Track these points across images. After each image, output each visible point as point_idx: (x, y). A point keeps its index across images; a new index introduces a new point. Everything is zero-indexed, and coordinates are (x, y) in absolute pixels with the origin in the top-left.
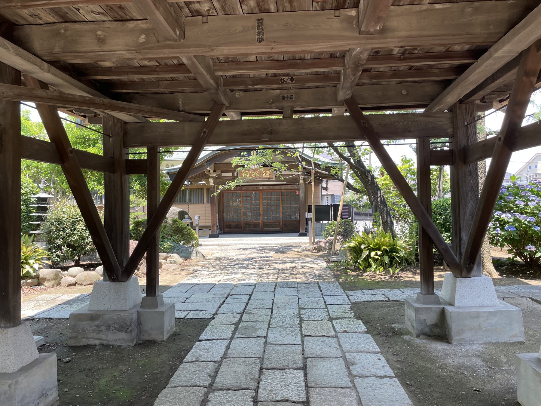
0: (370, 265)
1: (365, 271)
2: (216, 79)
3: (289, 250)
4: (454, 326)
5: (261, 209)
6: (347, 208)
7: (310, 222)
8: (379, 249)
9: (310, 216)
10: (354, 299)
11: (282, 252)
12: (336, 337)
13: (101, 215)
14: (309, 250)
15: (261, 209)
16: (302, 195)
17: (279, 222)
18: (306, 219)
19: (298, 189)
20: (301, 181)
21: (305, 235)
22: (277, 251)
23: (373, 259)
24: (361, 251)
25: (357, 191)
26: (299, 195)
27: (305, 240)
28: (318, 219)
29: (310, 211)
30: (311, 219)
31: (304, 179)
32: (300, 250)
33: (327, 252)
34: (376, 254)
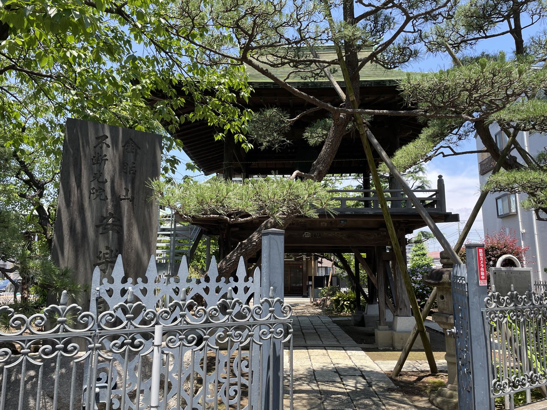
0: (344, 309)
1: (341, 312)
2: (28, 16)
6: (335, 279)
7: (310, 287)
13: (272, 81)
19: (302, 265)
20: (304, 259)
21: (307, 297)
23: (346, 305)
24: (340, 301)
25: (341, 268)
26: (302, 268)
27: (307, 300)
28: (316, 286)
30: (311, 285)
32: (304, 305)
33: (322, 305)
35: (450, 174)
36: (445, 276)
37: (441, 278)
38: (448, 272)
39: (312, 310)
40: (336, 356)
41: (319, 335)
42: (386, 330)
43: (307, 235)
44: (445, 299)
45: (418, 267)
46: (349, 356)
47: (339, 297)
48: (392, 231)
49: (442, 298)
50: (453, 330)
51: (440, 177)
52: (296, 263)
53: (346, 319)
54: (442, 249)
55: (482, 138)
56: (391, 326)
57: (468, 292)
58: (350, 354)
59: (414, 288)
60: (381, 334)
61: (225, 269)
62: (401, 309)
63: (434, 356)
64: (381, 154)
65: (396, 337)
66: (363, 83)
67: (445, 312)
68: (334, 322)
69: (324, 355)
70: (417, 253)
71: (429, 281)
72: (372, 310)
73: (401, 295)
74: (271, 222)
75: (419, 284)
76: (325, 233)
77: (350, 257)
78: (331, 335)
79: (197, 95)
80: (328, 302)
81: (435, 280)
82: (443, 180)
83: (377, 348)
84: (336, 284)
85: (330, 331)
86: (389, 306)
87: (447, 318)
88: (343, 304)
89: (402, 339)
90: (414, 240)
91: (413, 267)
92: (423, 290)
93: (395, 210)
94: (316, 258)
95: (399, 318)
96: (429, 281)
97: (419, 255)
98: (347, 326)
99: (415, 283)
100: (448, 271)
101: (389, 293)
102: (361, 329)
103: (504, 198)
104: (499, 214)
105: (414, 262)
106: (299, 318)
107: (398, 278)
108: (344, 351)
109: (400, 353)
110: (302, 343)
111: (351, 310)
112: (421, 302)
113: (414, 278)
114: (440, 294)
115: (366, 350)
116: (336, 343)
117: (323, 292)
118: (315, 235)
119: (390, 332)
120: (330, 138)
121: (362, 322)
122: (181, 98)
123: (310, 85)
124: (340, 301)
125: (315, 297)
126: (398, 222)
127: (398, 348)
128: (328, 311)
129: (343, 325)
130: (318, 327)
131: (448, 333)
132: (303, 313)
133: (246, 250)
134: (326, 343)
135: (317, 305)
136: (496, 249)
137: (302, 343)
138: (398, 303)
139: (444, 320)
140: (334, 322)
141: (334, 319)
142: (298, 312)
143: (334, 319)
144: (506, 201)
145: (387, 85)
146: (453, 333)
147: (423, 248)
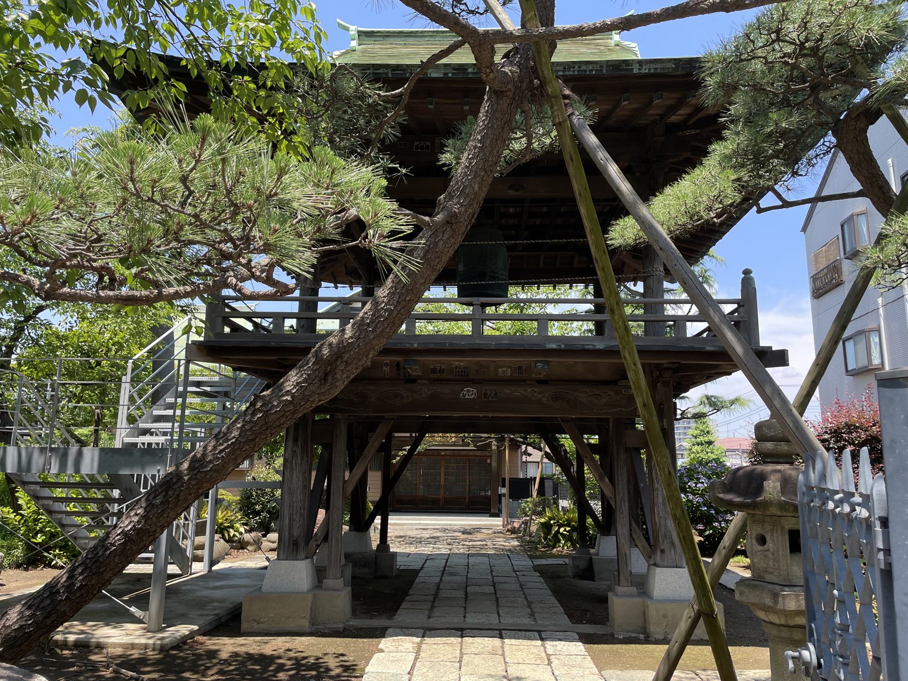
0: (559, 541)
1: (554, 547)
3: (478, 532)
4: (596, 568)
5: (442, 480)
7: (503, 499)
8: (568, 525)
9: (503, 491)
10: (536, 563)
11: (470, 533)
12: (515, 571)
14: (501, 532)
15: (442, 480)
16: (494, 464)
17: (465, 498)
18: (500, 495)
19: (490, 457)
20: (494, 447)
22: (464, 533)
23: (562, 534)
24: (551, 526)
27: (497, 522)
29: (504, 486)
30: (504, 495)
31: (498, 447)
34: (565, 530)
35: (772, 267)
36: (772, 487)
37: (760, 489)
38: (779, 475)
39: (501, 542)
40: (519, 656)
41: (497, 599)
42: (631, 596)
43: (470, 393)
44: (770, 544)
45: (700, 463)
46: (548, 656)
47: (550, 519)
48: (636, 373)
49: (762, 540)
50: (805, 654)
51: (747, 272)
52: (479, 453)
53: (560, 561)
54: (765, 414)
55: (850, 160)
56: (642, 585)
57: (887, 551)
58: (550, 651)
59: (693, 504)
60: (621, 605)
61: (211, 462)
62: (663, 551)
63: (734, 658)
64: (606, 169)
65: (653, 611)
66: (584, 67)
67: (768, 578)
68: (536, 568)
69: (493, 653)
70: (698, 440)
71: (729, 497)
72: (606, 547)
73: (663, 522)
74: (330, 345)
75: (702, 495)
76: (506, 391)
77: (567, 442)
78: (521, 600)
79: (214, 78)
80: (534, 528)
81: (745, 494)
82: (752, 279)
83: (612, 635)
84: (551, 493)
85: (522, 589)
86: (639, 545)
87: (775, 596)
88: (558, 532)
89: (665, 616)
90: (692, 411)
91: (691, 464)
92: (710, 507)
93: (653, 342)
94: (515, 446)
95: (658, 570)
96: (729, 497)
97: (702, 444)
98: (560, 577)
99: (694, 495)
100: (779, 471)
101: (639, 517)
102: (586, 584)
103: (858, 338)
104: (849, 369)
105: (692, 456)
106: (472, 560)
107: (656, 485)
108: (539, 643)
109: (660, 650)
110: (456, 620)
111: (572, 544)
112: (705, 530)
113: (692, 484)
114: (754, 531)
115: (587, 639)
116: (527, 621)
117: (525, 508)
118: (485, 394)
119: (640, 600)
120: (479, 133)
121: (588, 572)
122: (178, 80)
123: (470, 70)
124: (551, 526)
125: (512, 515)
126: (658, 366)
127: (657, 637)
128: (530, 546)
129: (549, 575)
130: (501, 579)
131: (791, 665)
132: (482, 547)
133: (266, 414)
134: (507, 620)
135: (513, 531)
136: (857, 428)
137: (456, 620)
138: (656, 538)
139: (768, 601)
140: (536, 568)
141: (538, 562)
142: (473, 547)
143: (538, 562)
144: (862, 345)
145: (635, 71)
146: (807, 665)
147: (708, 432)
